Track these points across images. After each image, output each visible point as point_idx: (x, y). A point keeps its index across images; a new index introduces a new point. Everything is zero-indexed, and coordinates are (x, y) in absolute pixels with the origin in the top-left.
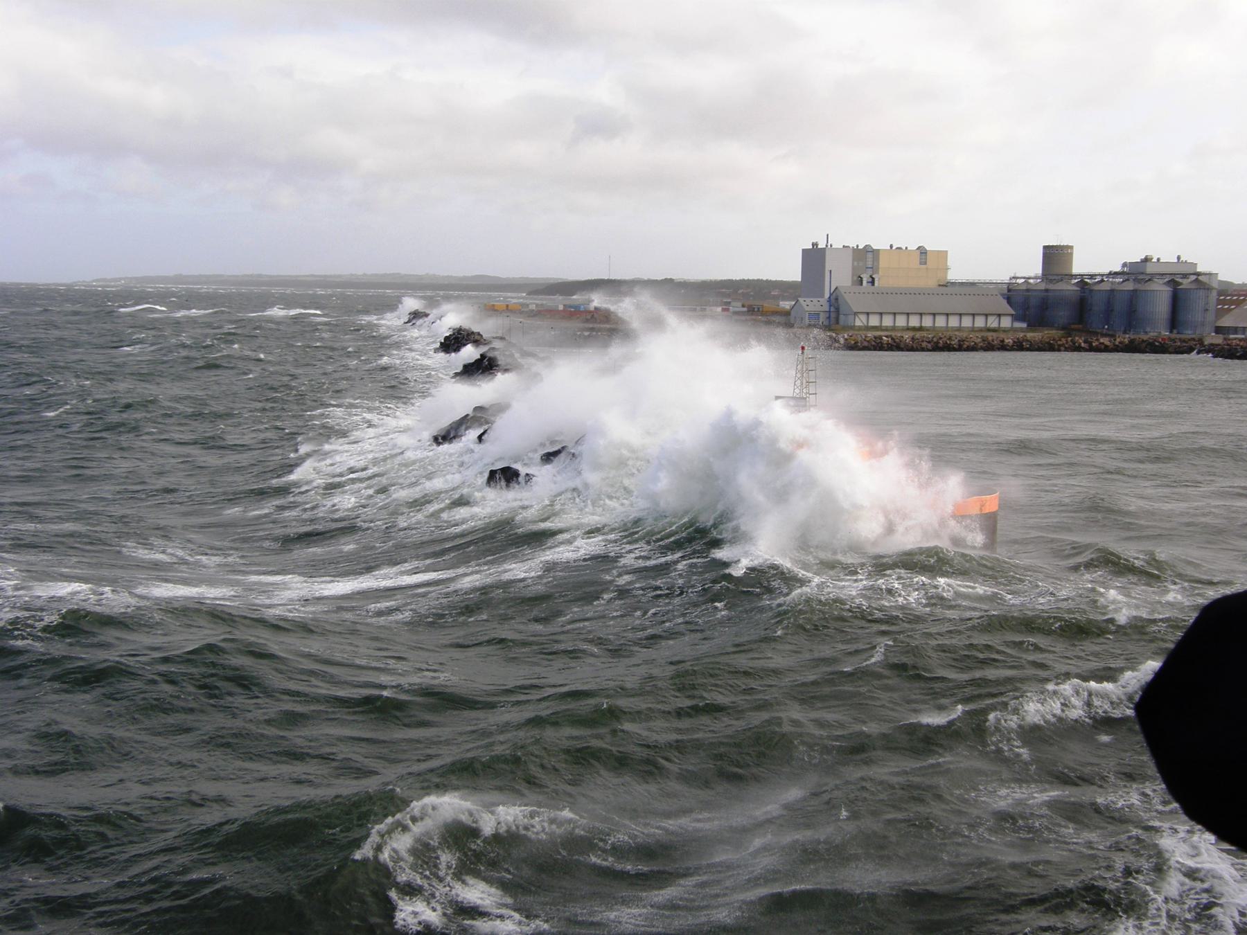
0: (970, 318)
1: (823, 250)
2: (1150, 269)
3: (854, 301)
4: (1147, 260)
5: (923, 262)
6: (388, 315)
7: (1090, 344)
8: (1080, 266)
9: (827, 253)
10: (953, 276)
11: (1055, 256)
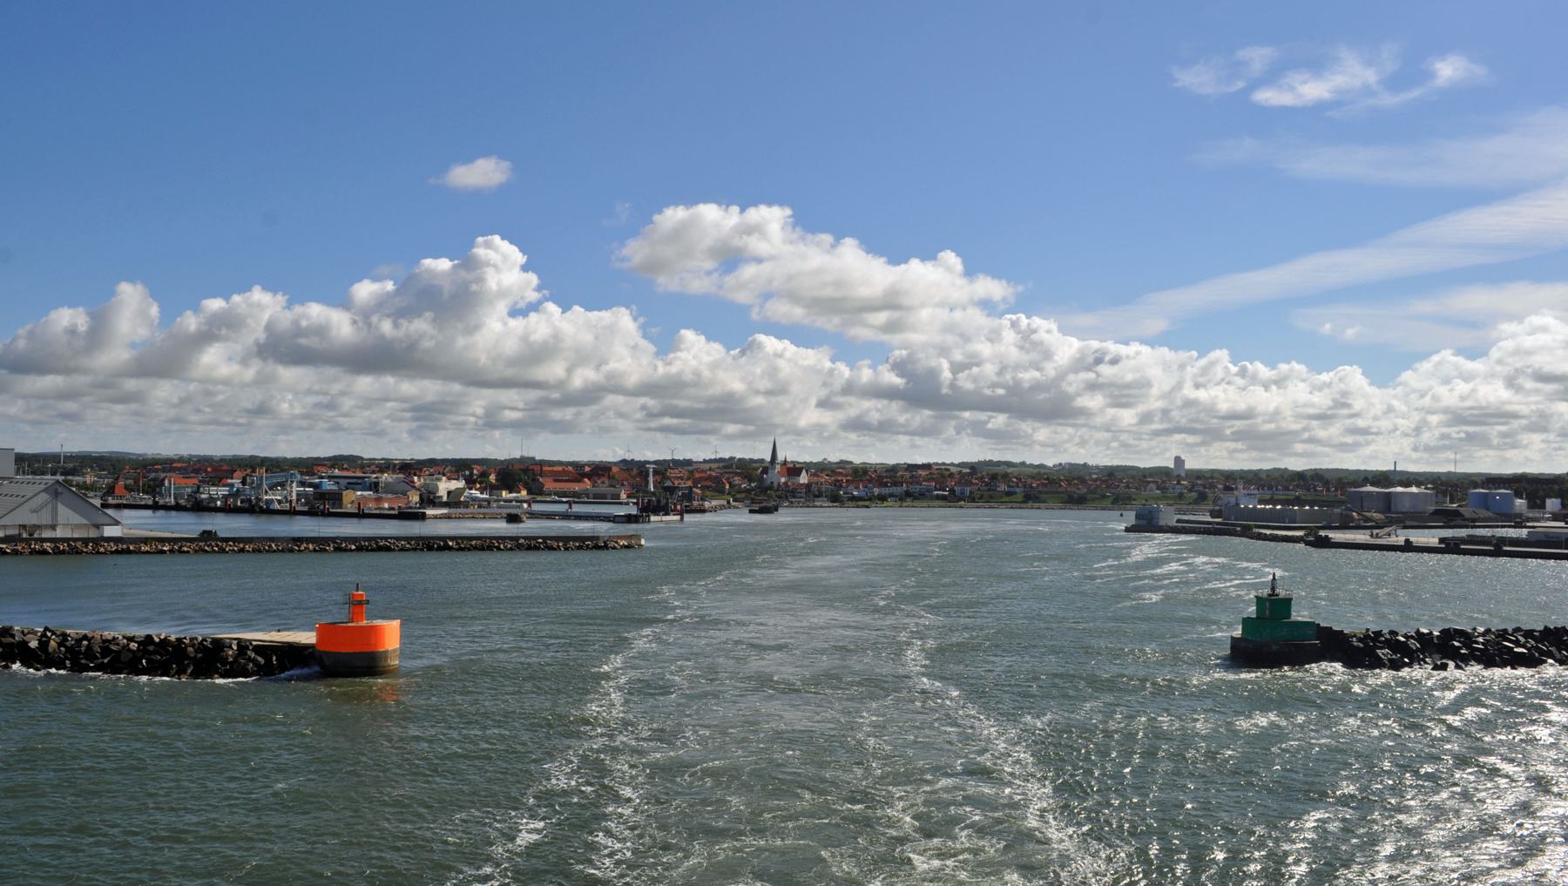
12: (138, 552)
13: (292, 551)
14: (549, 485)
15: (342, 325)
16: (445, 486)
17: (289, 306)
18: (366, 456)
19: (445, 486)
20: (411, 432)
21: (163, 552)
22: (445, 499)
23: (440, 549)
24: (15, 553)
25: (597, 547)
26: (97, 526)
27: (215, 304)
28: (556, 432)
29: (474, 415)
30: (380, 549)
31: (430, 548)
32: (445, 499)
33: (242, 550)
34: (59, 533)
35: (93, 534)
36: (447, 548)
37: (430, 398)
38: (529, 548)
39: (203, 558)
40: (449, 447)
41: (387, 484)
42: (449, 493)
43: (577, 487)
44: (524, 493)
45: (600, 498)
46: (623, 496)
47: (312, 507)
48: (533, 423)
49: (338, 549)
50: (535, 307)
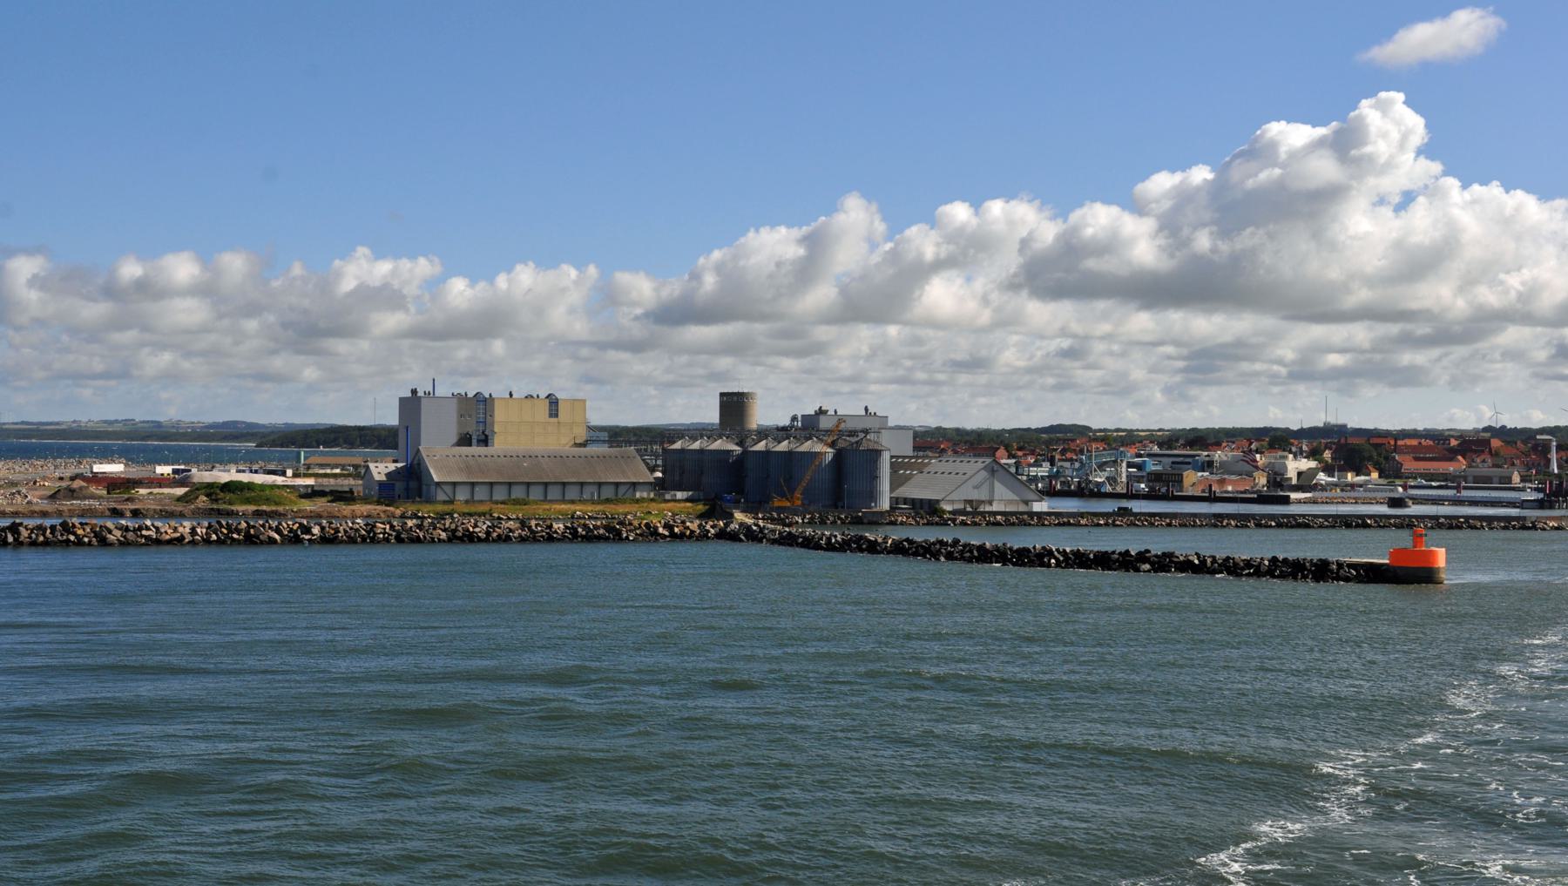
5: (554, 413)
8: (767, 413)
12: (1078, 525)
13: (1216, 526)
14: (1409, 465)
15: (1142, 246)
16: (1294, 466)
17: (1065, 221)
18: (1094, 426)
19: (1294, 466)
20: (1167, 390)
21: (1098, 525)
22: (1294, 481)
23: (1358, 526)
24: (975, 524)
25: (1524, 528)
26: (1026, 503)
27: (959, 213)
28: (1395, 384)
29: (1280, 362)
30: (1299, 526)
31: (1348, 526)
32: (1294, 481)
33: (1169, 525)
34: (995, 507)
35: (1022, 508)
36: (1365, 526)
37: (1227, 338)
38: (1451, 527)
39: (1133, 530)
40: (1216, 410)
41: (1222, 464)
42: (1300, 474)
43: (1450, 468)
44: (1375, 475)
45: (1483, 481)
46: (1516, 478)
47: (1152, 489)
48: (1370, 369)
49: (1259, 525)
50: (1430, 190)
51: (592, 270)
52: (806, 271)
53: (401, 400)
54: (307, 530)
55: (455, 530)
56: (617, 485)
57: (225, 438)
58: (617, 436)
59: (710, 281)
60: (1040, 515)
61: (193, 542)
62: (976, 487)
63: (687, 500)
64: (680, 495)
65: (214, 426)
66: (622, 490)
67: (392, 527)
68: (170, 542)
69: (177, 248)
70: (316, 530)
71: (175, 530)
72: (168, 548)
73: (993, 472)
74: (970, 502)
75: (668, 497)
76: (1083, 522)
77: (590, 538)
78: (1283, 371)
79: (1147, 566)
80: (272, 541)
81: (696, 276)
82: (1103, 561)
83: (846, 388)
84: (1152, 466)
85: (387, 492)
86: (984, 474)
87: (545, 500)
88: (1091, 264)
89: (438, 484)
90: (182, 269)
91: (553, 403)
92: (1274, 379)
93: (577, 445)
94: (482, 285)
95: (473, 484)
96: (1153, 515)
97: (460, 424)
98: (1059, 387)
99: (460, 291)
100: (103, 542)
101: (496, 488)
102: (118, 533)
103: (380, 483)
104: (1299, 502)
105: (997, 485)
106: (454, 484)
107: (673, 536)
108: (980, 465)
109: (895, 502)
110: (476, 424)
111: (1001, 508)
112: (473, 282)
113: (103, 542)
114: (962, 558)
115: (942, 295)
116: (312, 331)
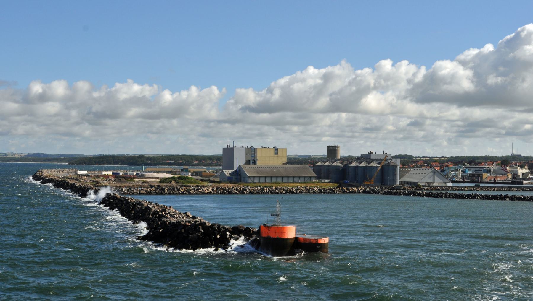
0: (298, 178)
1: (233, 149)
2: (372, 157)
3: (249, 171)
4: (371, 153)
5: (276, 153)
6: (408, 123)
7: (349, 190)
8: (342, 153)
9: (235, 151)
10: (326, 154)
11: (332, 150)
16: (521, 171)
19: (521, 171)
20: (449, 140)
22: (521, 177)
27: (387, 65)
29: (504, 128)
32: (521, 177)
34: (435, 184)
35: (444, 185)
42: (523, 174)
51: (224, 90)
52: (319, 90)
53: (223, 149)
54: (246, 190)
55: (287, 190)
56: (305, 177)
57: (34, 160)
58: (291, 161)
59: (277, 94)
60: (449, 187)
61: (214, 193)
62: (429, 178)
63: (329, 182)
64: (327, 181)
65: (29, 155)
66: (306, 179)
67: (269, 189)
68: (207, 193)
69: (58, 78)
70: (248, 190)
71: (208, 190)
72: (206, 195)
73: (434, 173)
74: (428, 183)
75: (323, 181)
76: (466, 189)
77: (326, 192)
78: (504, 132)
79: (508, 199)
80: (236, 193)
81: (270, 91)
82: (494, 197)
83: (314, 139)
84: (469, 172)
85: (230, 180)
86: (432, 173)
87: (288, 182)
88: (445, 88)
89: (249, 177)
90: (59, 88)
91: (276, 149)
92: (499, 135)
93: (284, 164)
94: (176, 95)
95: (260, 177)
96: (489, 187)
97: (246, 157)
98: (404, 138)
99: (167, 96)
100: (190, 193)
101: (290, 178)
102: (193, 191)
103: (228, 177)
104: (526, 184)
105: (436, 178)
106: (254, 177)
107: (350, 192)
108: (430, 171)
109: (401, 182)
110: (252, 155)
111: (437, 185)
112: (173, 92)
113: (190, 193)
114: (450, 197)
115: (372, 101)
116: (102, 115)
